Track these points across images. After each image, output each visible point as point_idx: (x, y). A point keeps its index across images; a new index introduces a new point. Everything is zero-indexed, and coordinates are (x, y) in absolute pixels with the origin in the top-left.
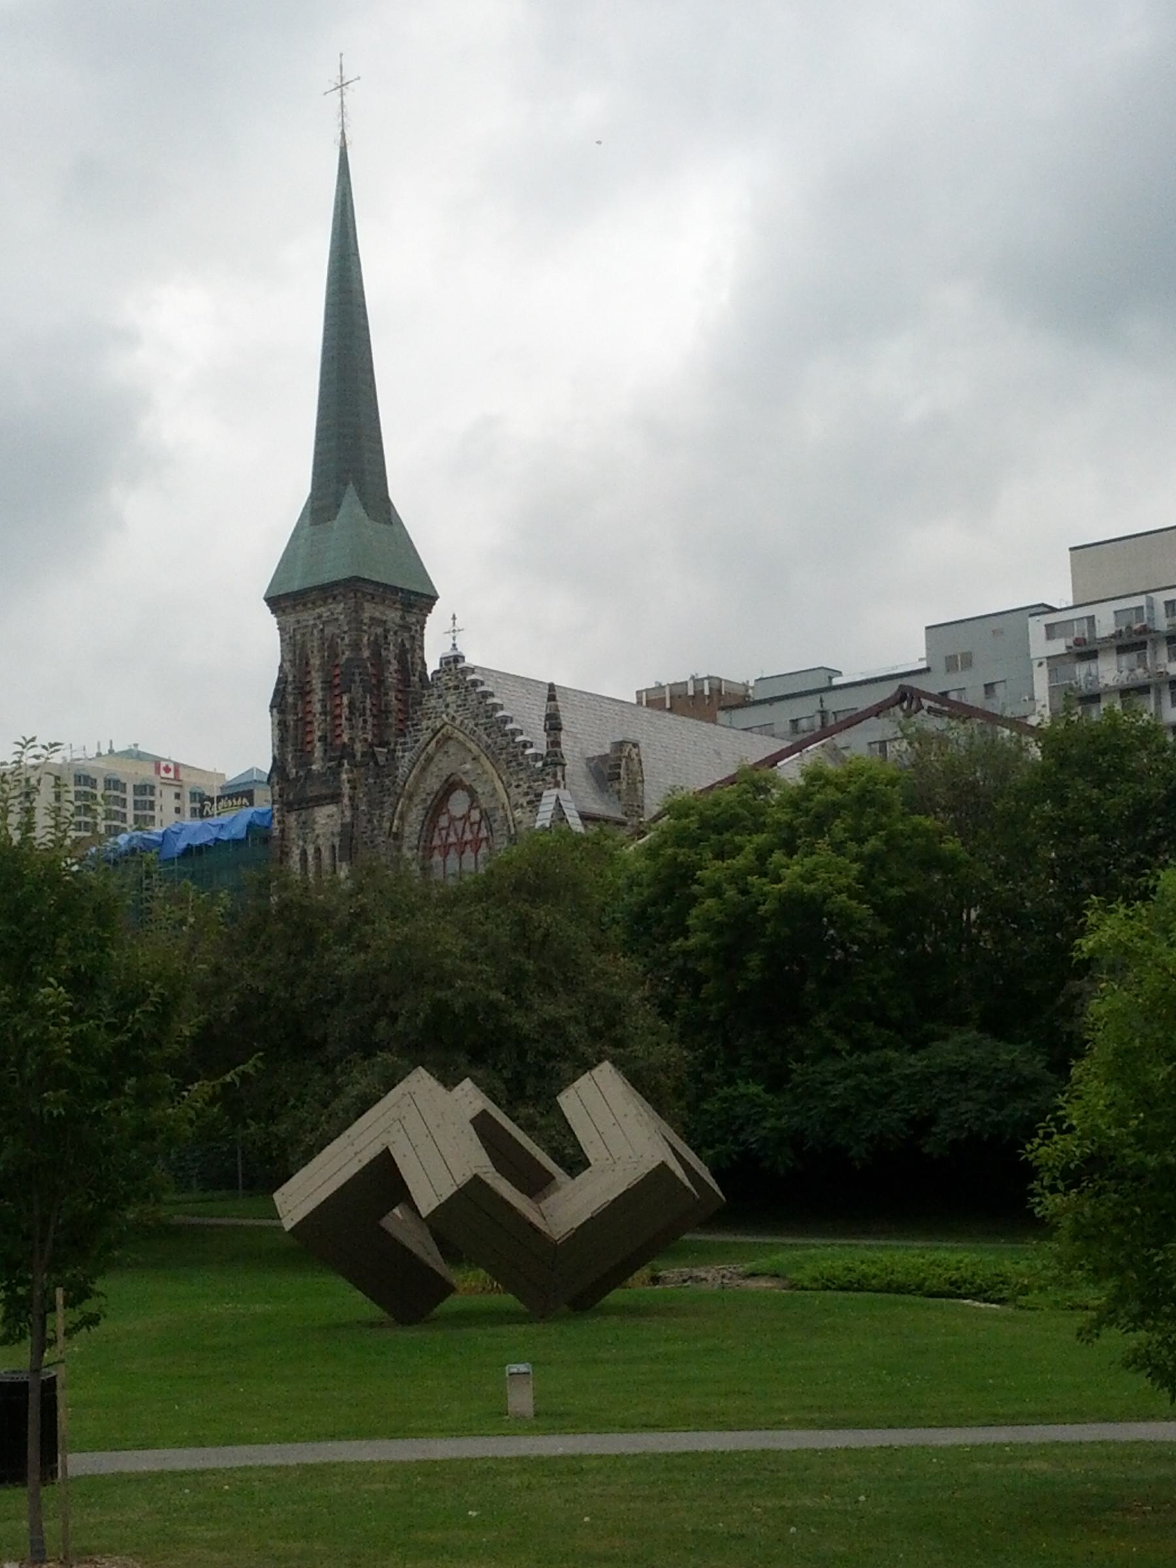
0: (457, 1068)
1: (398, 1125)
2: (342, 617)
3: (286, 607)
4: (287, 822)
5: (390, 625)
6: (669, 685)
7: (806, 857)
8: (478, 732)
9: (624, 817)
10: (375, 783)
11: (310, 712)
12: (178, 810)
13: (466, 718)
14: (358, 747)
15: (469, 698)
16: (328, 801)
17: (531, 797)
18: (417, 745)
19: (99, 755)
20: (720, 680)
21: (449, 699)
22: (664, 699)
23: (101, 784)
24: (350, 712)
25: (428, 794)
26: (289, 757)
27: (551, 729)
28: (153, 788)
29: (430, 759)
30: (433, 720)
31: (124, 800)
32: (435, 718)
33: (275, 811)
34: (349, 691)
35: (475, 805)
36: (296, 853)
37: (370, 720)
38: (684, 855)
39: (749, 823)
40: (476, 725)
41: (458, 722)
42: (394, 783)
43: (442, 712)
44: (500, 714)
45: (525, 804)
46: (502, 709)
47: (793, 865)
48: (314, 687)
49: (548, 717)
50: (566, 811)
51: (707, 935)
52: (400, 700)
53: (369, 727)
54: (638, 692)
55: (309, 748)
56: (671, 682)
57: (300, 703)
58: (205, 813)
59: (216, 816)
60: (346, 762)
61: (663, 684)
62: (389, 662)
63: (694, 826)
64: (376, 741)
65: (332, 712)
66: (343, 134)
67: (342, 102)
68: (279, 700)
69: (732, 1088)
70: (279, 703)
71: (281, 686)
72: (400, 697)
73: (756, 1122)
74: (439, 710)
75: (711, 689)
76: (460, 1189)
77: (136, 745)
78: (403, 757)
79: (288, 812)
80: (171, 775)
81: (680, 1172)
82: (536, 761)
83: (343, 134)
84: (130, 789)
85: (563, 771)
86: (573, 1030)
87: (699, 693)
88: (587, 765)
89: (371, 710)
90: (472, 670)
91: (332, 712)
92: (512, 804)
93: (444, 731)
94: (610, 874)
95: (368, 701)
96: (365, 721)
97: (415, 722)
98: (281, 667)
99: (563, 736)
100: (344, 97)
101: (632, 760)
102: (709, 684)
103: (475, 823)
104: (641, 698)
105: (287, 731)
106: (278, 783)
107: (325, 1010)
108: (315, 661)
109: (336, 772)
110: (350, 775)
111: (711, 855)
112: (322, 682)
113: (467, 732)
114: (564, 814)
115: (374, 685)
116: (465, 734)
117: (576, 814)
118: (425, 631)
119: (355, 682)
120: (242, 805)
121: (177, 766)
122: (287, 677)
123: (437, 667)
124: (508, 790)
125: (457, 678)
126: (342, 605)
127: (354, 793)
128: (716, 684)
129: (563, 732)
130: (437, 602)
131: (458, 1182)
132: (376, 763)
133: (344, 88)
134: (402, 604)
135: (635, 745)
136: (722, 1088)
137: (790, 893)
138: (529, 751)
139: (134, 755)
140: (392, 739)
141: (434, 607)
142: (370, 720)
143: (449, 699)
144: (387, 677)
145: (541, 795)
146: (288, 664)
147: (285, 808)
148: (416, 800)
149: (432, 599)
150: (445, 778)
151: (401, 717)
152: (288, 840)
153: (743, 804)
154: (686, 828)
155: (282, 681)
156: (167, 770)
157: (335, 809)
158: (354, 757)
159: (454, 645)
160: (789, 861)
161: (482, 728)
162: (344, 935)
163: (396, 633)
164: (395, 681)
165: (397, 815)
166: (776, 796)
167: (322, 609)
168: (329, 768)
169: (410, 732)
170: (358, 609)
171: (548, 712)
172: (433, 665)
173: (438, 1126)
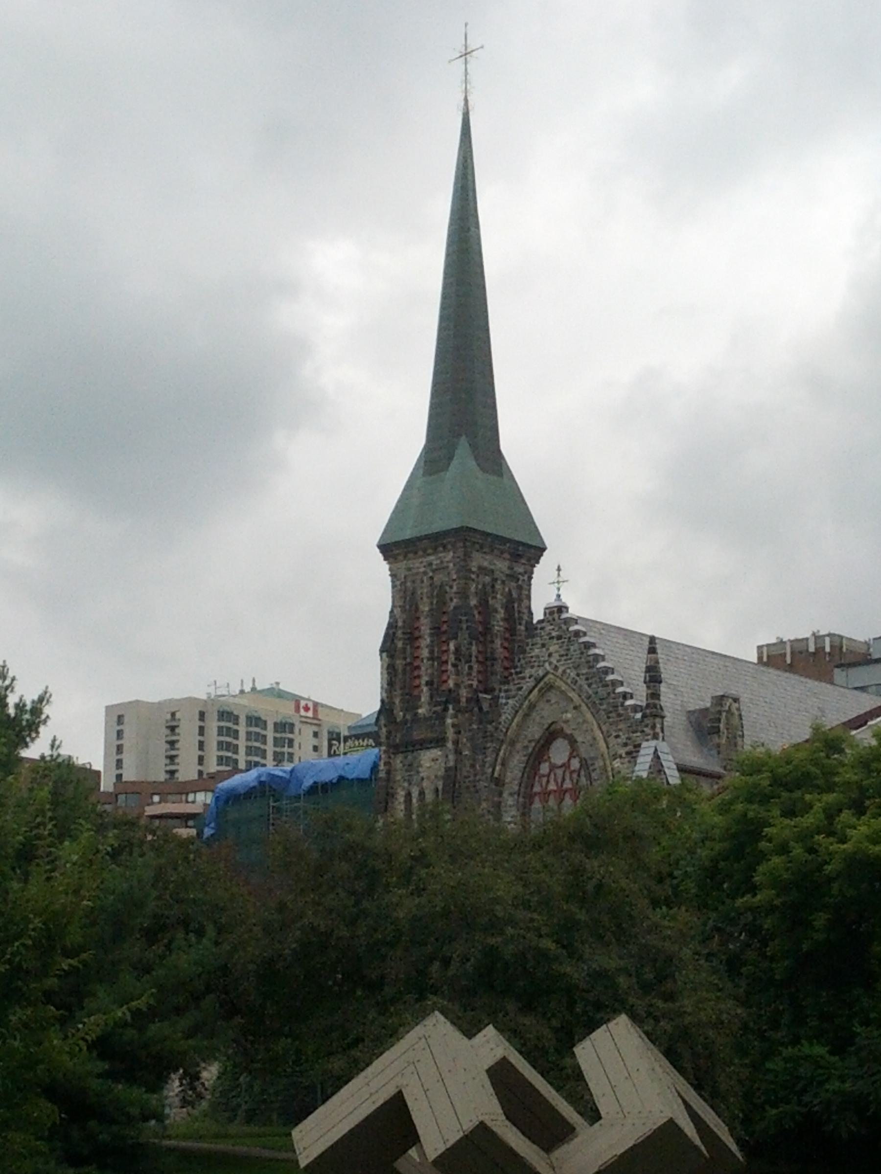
0: (507, 1014)
1: (412, 1067)
2: (451, 565)
3: (398, 554)
4: (393, 764)
5: (497, 574)
6: (789, 640)
7: (874, 818)
8: (579, 682)
9: (722, 771)
10: (478, 728)
11: (417, 657)
12: (316, 748)
13: (569, 668)
14: (464, 693)
15: (572, 648)
16: (433, 745)
17: (630, 748)
18: (520, 693)
19: (242, 692)
20: (841, 637)
21: (552, 649)
22: (785, 655)
23: (243, 720)
24: (456, 659)
25: (530, 741)
26: (397, 701)
27: (650, 681)
28: (292, 725)
29: (532, 707)
30: (535, 669)
31: (265, 737)
32: (539, 666)
33: (382, 753)
34: (456, 638)
35: (575, 754)
36: (401, 795)
37: (476, 666)
38: (754, 811)
39: (819, 782)
40: (578, 675)
41: (560, 670)
42: (497, 729)
43: (544, 662)
44: (602, 664)
45: (624, 755)
46: (604, 659)
47: (860, 825)
48: (422, 632)
49: (649, 669)
50: (664, 763)
51: (773, 892)
52: (505, 648)
53: (474, 674)
54: (760, 648)
55: (416, 693)
56: (792, 638)
57: (408, 647)
58: (332, 752)
59: (342, 756)
60: (451, 707)
61: (784, 640)
62: (496, 611)
63: (766, 783)
64: (481, 688)
65: (439, 658)
66: (466, 100)
67: (466, 70)
68: (389, 644)
69: (796, 1049)
70: (388, 648)
71: (391, 632)
72: (506, 645)
73: (821, 1084)
74: (542, 659)
75: (831, 647)
76: (466, 1136)
77: (278, 683)
78: (506, 704)
79: (393, 753)
80: (310, 714)
81: (689, 1129)
82: (636, 712)
83: (466, 100)
84: (270, 726)
85: (662, 724)
86: (622, 981)
87: (820, 650)
88: (688, 718)
89: (477, 657)
90: (575, 621)
91: (439, 658)
92: (611, 754)
93: (546, 679)
94: (687, 827)
95: (474, 648)
96: (470, 668)
97: (518, 670)
98: (392, 612)
99: (663, 688)
100: (468, 66)
101: (733, 714)
102: (831, 642)
103: (574, 771)
104: (762, 653)
105: (395, 676)
106: (385, 726)
107: (384, 950)
108: (425, 608)
109: (440, 717)
110: (455, 720)
111: (778, 813)
112: (431, 629)
113: (569, 681)
114: (662, 766)
115: (480, 633)
116: (566, 683)
117: (675, 767)
118: (533, 581)
119: (461, 629)
120: (367, 746)
121: (316, 705)
122: (397, 622)
123: (541, 617)
124: (608, 739)
125: (560, 628)
126: (451, 554)
127: (458, 738)
128: (837, 641)
129: (663, 685)
130: (545, 553)
131: (465, 1128)
132: (481, 709)
133: (468, 56)
134: (510, 553)
135: (736, 700)
136: (787, 1048)
137: (855, 853)
138: (629, 702)
139: (276, 693)
140: (497, 686)
141: (542, 558)
142: (476, 666)
143: (552, 649)
144: (493, 626)
145: (639, 745)
146: (399, 609)
147: (391, 751)
148: (519, 746)
149: (541, 550)
150: (546, 726)
151: (506, 664)
152: (395, 782)
153: (815, 762)
154: (756, 785)
155: (392, 626)
156: (307, 709)
157: (440, 753)
158: (459, 702)
159: (559, 596)
160: (857, 822)
161: (583, 677)
162: (406, 876)
163: (503, 582)
164: (502, 629)
165: (499, 761)
166: (849, 756)
167: (432, 558)
168: (435, 712)
169: (513, 680)
170: (467, 556)
171: (648, 664)
172: (538, 615)
173: (450, 1071)
